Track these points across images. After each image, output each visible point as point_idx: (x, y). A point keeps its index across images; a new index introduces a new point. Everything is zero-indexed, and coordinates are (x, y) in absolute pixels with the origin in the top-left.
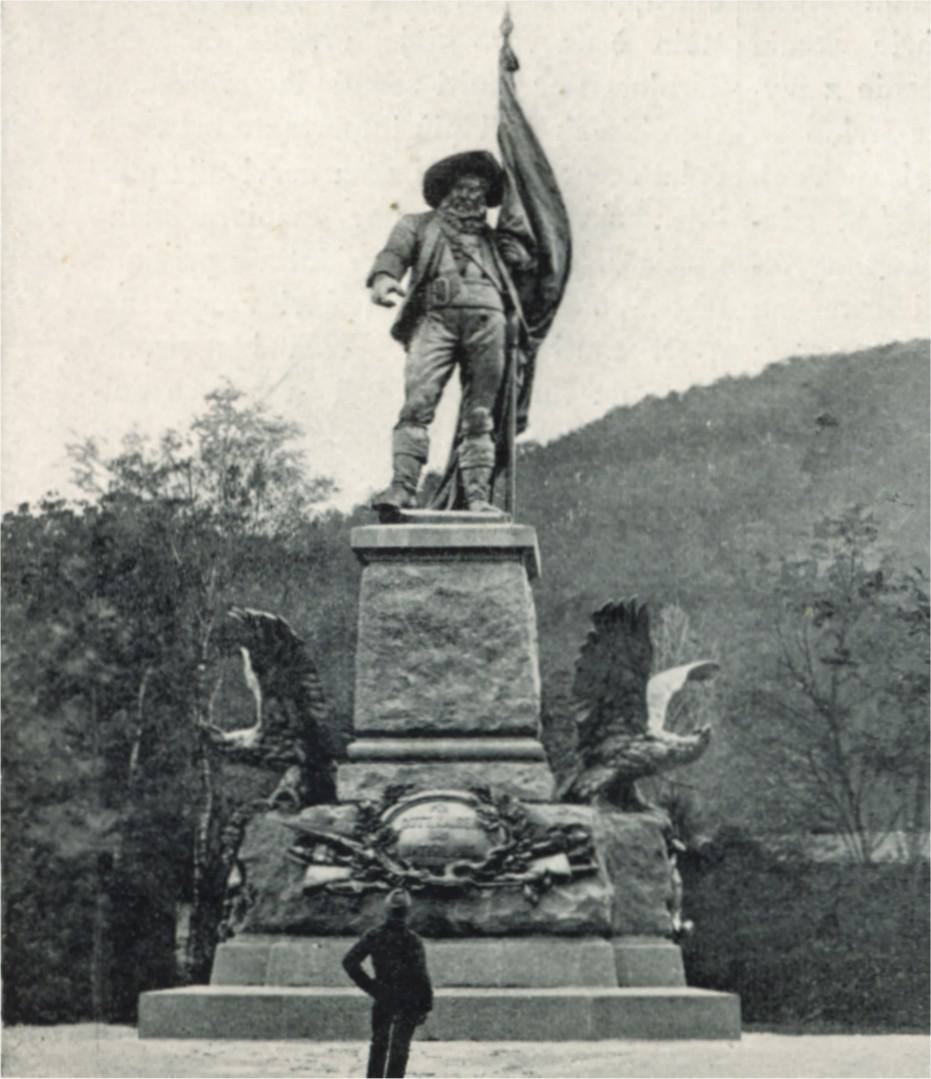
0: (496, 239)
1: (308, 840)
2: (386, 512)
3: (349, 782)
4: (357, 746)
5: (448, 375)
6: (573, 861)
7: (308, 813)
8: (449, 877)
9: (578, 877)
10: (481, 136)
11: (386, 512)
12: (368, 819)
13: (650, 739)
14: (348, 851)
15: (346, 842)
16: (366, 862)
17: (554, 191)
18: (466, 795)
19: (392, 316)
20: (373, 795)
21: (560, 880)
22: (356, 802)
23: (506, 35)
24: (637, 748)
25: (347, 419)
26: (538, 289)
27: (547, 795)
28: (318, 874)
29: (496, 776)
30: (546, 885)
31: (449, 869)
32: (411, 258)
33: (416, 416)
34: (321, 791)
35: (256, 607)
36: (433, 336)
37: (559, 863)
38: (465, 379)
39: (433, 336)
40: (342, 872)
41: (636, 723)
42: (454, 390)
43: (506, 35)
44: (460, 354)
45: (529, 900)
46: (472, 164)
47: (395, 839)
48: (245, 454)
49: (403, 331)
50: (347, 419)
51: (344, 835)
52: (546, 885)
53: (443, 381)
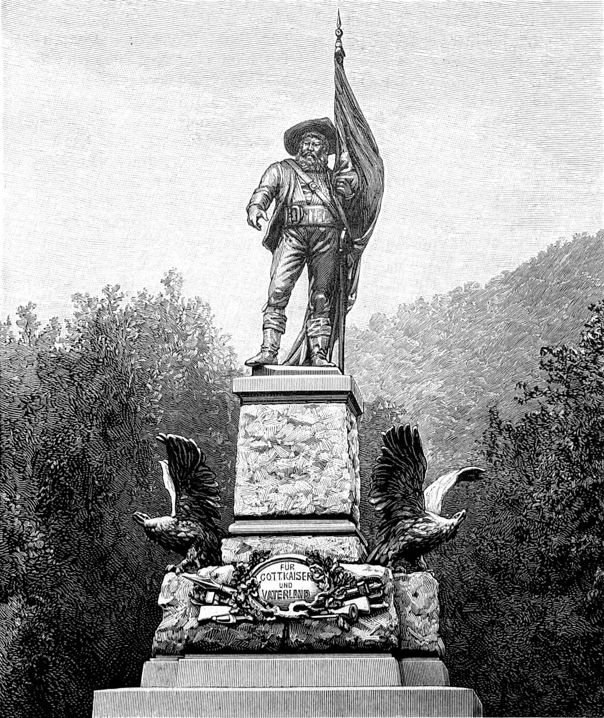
0: (331, 178)
1: (201, 588)
2: (258, 368)
3: (229, 549)
4: (232, 528)
5: (298, 275)
6: (371, 602)
7: (204, 572)
8: (291, 613)
9: (374, 613)
10: (324, 109)
11: (258, 368)
12: (241, 573)
13: (428, 521)
14: (227, 596)
15: (228, 590)
16: (240, 604)
17: (369, 138)
18: (304, 558)
19: (263, 234)
20: (246, 556)
21: (362, 614)
22: (234, 564)
23: (339, 37)
24: (421, 529)
25: (233, 294)
26: (357, 213)
27: (356, 556)
28: (206, 612)
29: (323, 545)
30: (355, 619)
31: (292, 606)
32: (275, 191)
33: (279, 301)
34: (213, 558)
35: (175, 434)
36: (288, 247)
37: (362, 603)
38: (311, 274)
39: (288, 247)
40: (225, 610)
41: (419, 513)
42: (303, 284)
43: (339, 37)
44: (305, 256)
45: (342, 629)
46: (319, 128)
47: (258, 587)
48: (169, 321)
49: (272, 243)
50: (233, 294)
51: (224, 584)
52: (355, 619)
53: (294, 279)
